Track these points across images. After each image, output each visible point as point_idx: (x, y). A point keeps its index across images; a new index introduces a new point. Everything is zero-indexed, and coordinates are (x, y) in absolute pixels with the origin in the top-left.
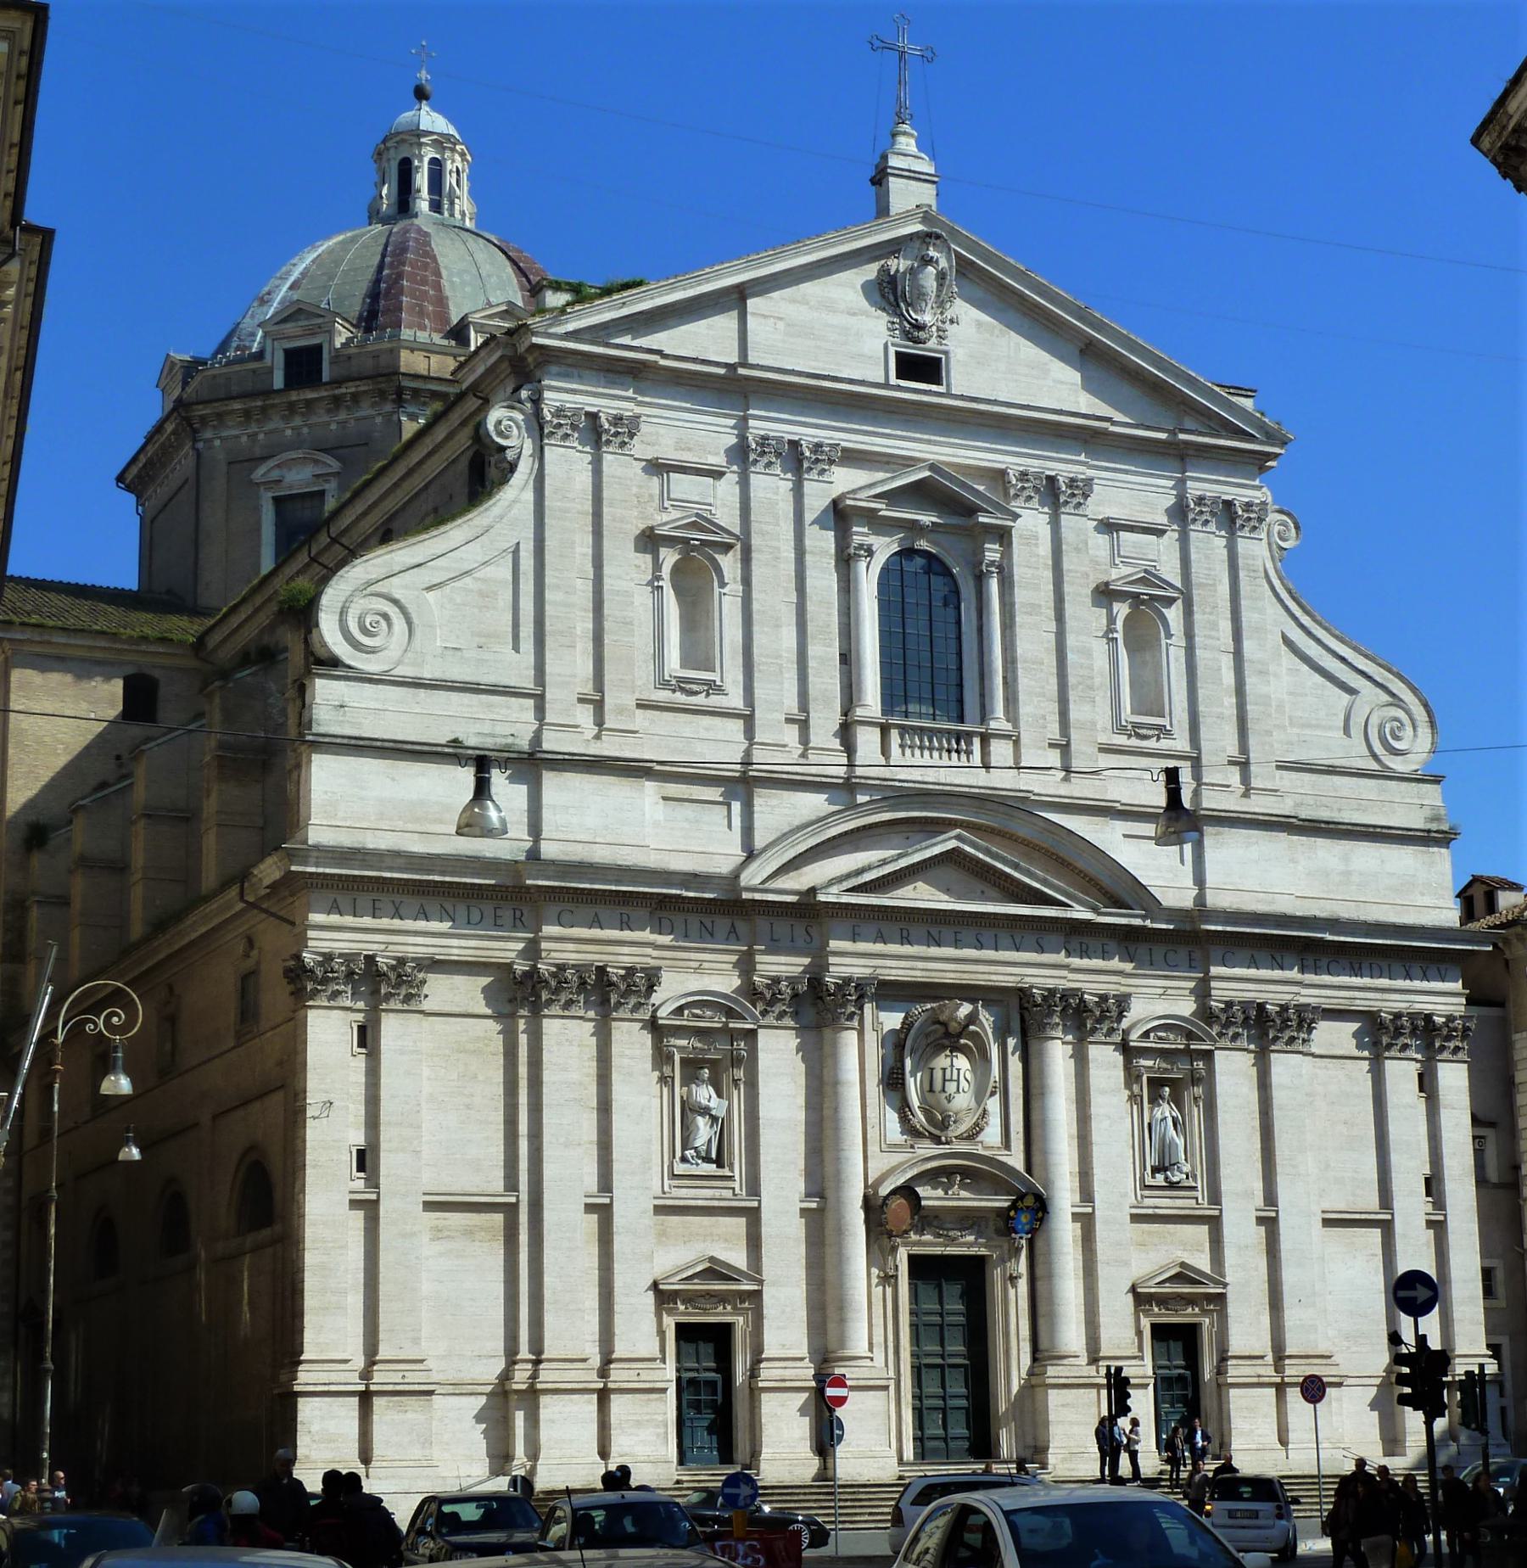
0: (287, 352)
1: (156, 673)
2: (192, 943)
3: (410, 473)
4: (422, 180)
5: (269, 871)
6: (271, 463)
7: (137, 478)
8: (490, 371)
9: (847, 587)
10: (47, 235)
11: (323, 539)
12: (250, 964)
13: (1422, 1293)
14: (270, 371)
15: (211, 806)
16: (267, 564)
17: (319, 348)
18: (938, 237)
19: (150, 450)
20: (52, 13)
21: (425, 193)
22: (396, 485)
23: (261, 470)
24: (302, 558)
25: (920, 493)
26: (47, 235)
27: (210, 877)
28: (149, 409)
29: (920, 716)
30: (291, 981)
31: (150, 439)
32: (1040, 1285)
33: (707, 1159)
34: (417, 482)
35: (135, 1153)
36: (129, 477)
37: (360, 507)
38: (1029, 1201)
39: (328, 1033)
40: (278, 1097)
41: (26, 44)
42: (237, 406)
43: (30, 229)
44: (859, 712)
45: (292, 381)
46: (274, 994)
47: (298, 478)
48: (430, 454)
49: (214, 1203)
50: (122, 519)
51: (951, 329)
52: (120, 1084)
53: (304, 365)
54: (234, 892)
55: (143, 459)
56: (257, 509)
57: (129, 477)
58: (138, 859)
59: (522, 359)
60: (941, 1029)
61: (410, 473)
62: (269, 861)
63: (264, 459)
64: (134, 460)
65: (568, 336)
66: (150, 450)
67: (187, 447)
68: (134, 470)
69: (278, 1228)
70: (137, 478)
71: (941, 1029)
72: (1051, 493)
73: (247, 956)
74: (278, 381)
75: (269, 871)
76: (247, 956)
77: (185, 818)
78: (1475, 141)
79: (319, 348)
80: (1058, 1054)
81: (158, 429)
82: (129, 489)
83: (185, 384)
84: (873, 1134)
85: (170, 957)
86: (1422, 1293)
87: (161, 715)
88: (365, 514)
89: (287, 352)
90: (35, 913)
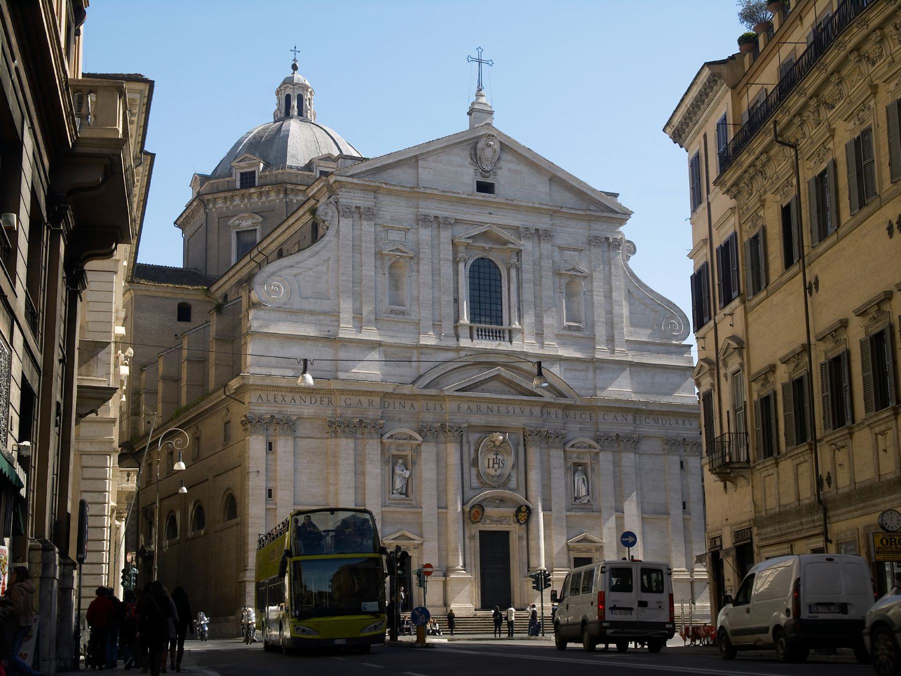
0: (242, 174)
1: (191, 303)
2: (206, 410)
3: (289, 227)
4: (295, 103)
5: (234, 384)
6: (235, 218)
7: (182, 223)
8: (319, 190)
9: (456, 273)
10: (153, 156)
11: (255, 252)
12: (228, 418)
13: (631, 539)
14: (235, 181)
15: (212, 356)
16: (234, 260)
17: (254, 172)
18: (493, 136)
19: (188, 212)
20: (155, 84)
21: (296, 108)
22: (284, 232)
23: (232, 221)
24: (248, 258)
25: (485, 235)
26: (153, 156)
27: (212, 385)
28: (188, 195)
29: (485, 323)
30: (244, 425)
31: (188, 207)
32: (531, 543)
33: (401, 493)
34: (292, 231)
35: (185, 490)
36: (179, 223)
37: (269, 240)
38: (524, 509)
39: (256, 445)
40: (239, 468)
41: (146, 94)
42: (221, 195)
43: (147, 153)
44: (461, 322)
45: (243, 186)
46: (236, 430)
47: (246, 224)
48: (296, 221)
49: (215, 510)
50: (177, 238)
51: (499, 172)
52: (181, 466)
53: (248, 180)
54: (222, 391)
55: (184, 215)
56: (230, 236)
57: (179, 223)
58: (184, 376)
59: (331, 186)
60: (492, 444)
61: (289, 227)
62: (235, 380)
63: (233, 216)
64: (182, 215)
65: (351, 176)
66: (188, 212)
67: (202, 211)
68: (181, 219)
69: (238, 519)
70: (182, 223)
71: (492, 444)
72: (540, 235)
73: (227, 415)
74: (238, 185)
75: (234, 384)
76: (227, 415)
77: (203, 361)
78: (664, 130)
79: (254, 172)
80: (534, 455)
81: (190, 204)
82: (179, 227)
83: (201, 186)
84: (466, 484)
85: (197, 415)
86: (631, 539)
87: (192, 319)
88: (271, 243)
89: (242, 174)
90: (143, 396)
